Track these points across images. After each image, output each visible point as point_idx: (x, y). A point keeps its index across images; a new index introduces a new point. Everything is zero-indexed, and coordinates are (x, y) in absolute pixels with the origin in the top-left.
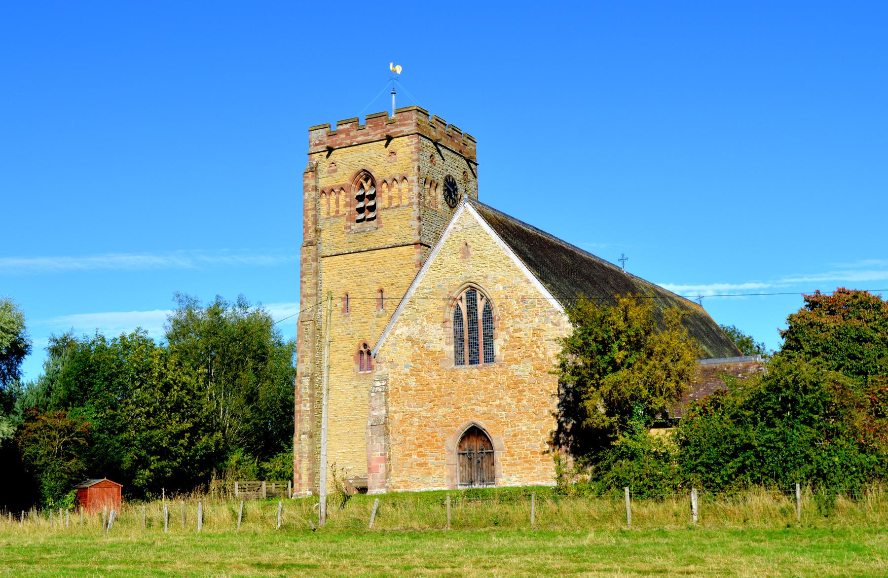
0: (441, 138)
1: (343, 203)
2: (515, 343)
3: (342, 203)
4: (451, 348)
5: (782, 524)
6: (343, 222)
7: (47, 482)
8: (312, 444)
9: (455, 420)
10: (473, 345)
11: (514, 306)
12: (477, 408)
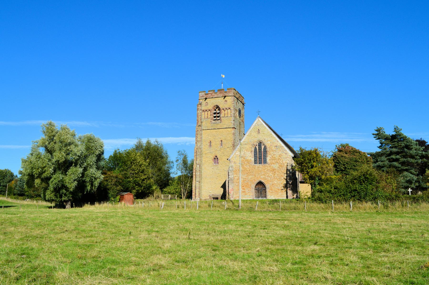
0: (239, 98)
1: (210, 115)
2: (273, 158)
3: (209, 114)
4: (253, 159)
5: (375, 211)
6: (210, 120)
7: (111, 193)
8: (199, 185)
9: (255, 180)
10: (260, 158)
11: (273, 148)
12: (261, 176)
